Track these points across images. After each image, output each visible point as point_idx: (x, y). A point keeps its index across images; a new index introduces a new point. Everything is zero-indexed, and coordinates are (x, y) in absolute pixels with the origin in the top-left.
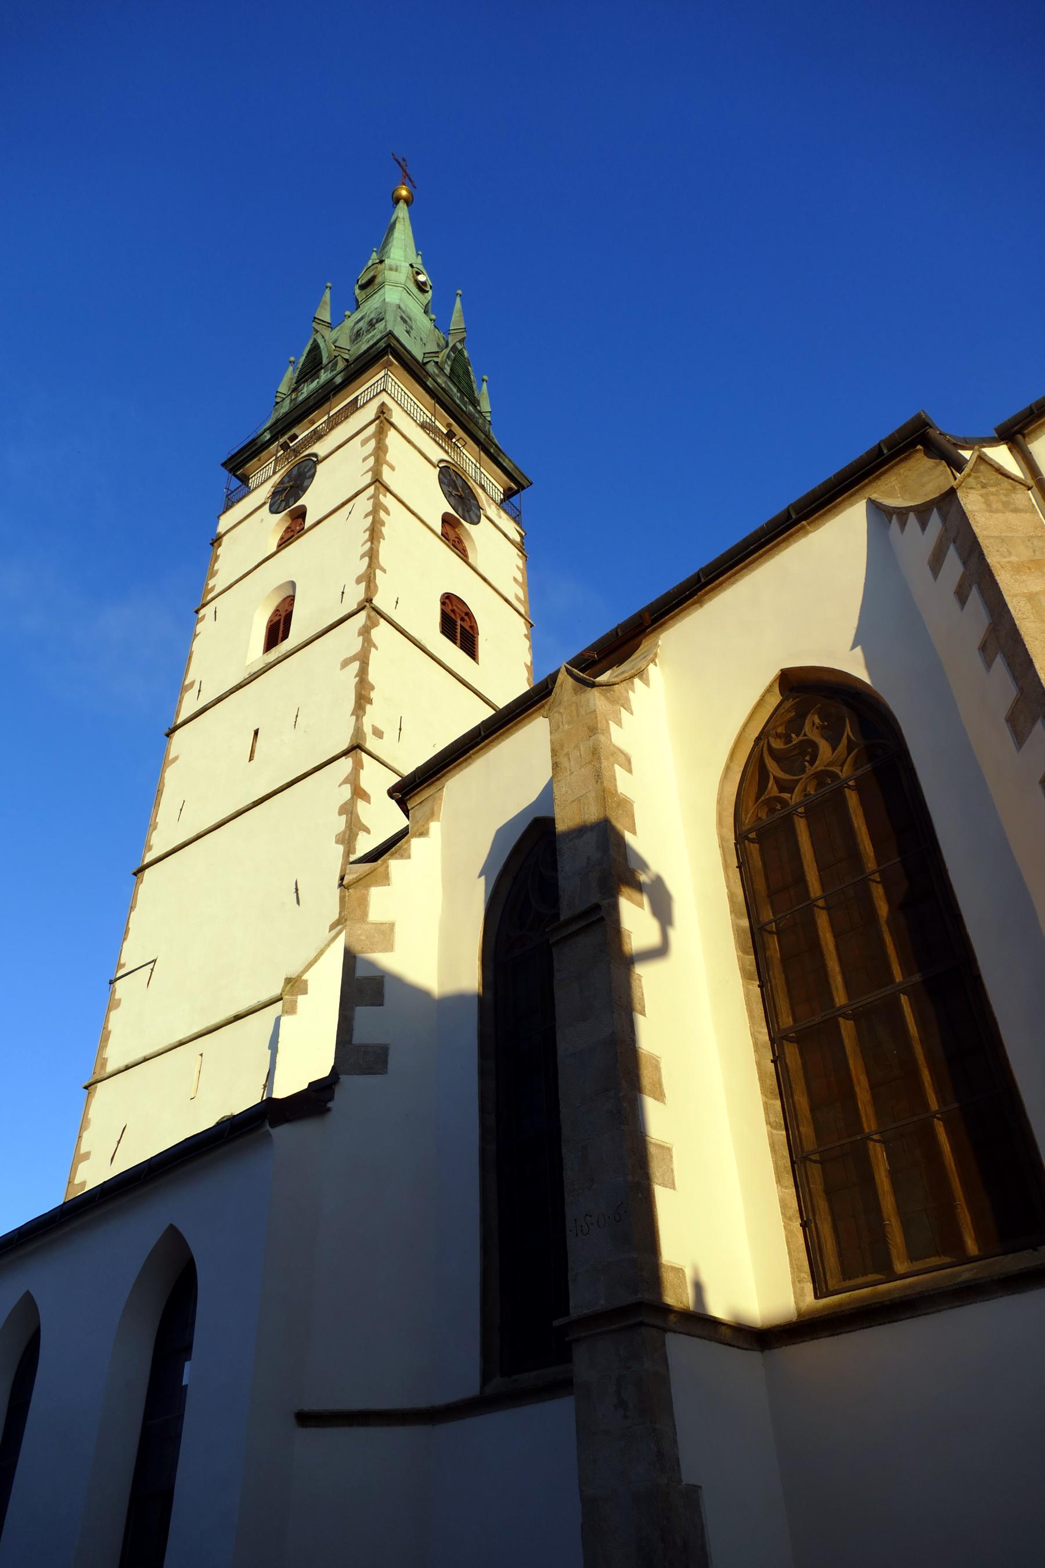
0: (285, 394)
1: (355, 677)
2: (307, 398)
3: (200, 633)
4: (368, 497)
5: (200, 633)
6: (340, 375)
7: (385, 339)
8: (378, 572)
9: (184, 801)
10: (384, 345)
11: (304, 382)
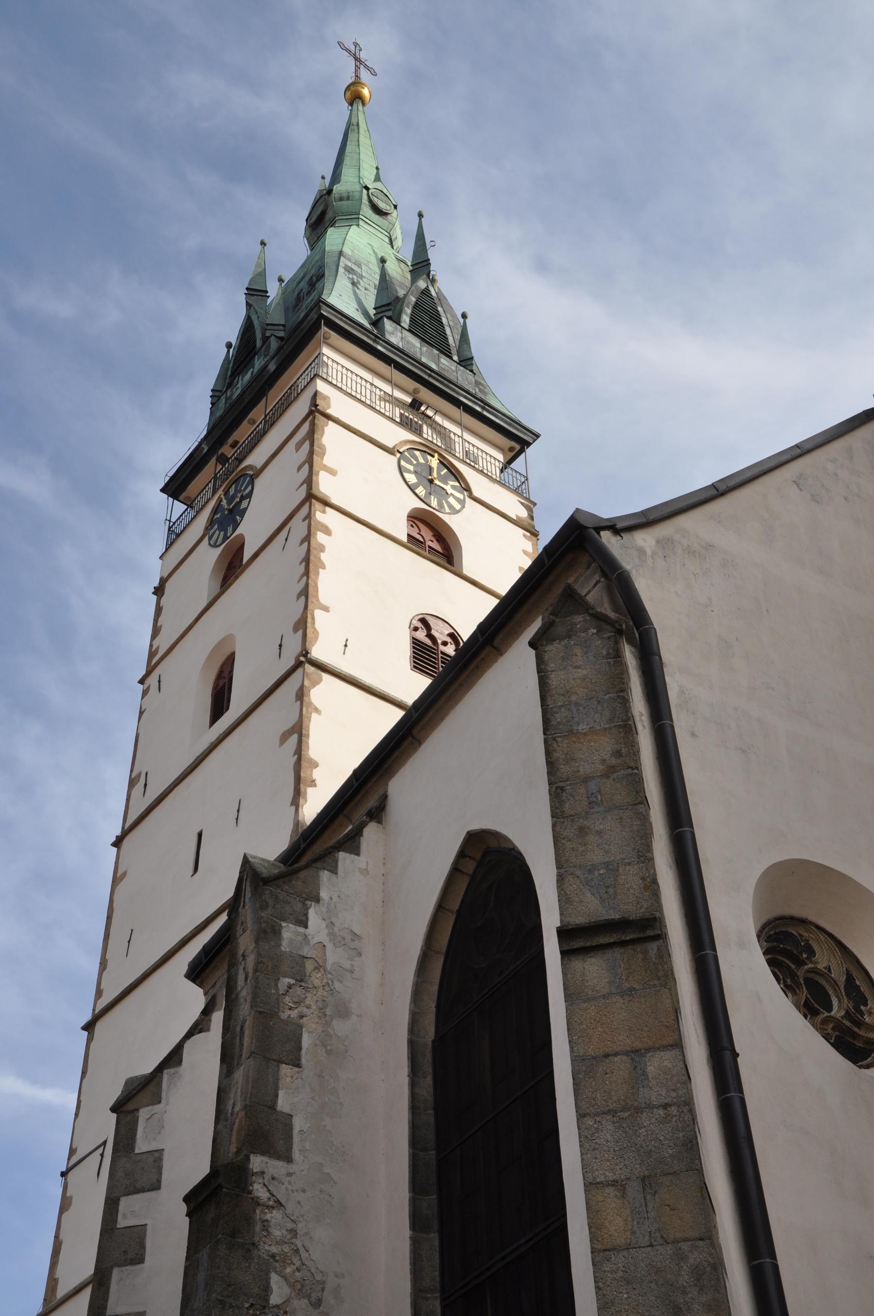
0: (220, 391)
1: (294, 756)
2: (242, 395)
3: (145, 710)
4: (303, 518)
5: (145, 710)
6: (273, 362)
7: (316, 308)
8: (318, 613)
9: (132, 930)
10: (316, 316)
11: (239, 375)
